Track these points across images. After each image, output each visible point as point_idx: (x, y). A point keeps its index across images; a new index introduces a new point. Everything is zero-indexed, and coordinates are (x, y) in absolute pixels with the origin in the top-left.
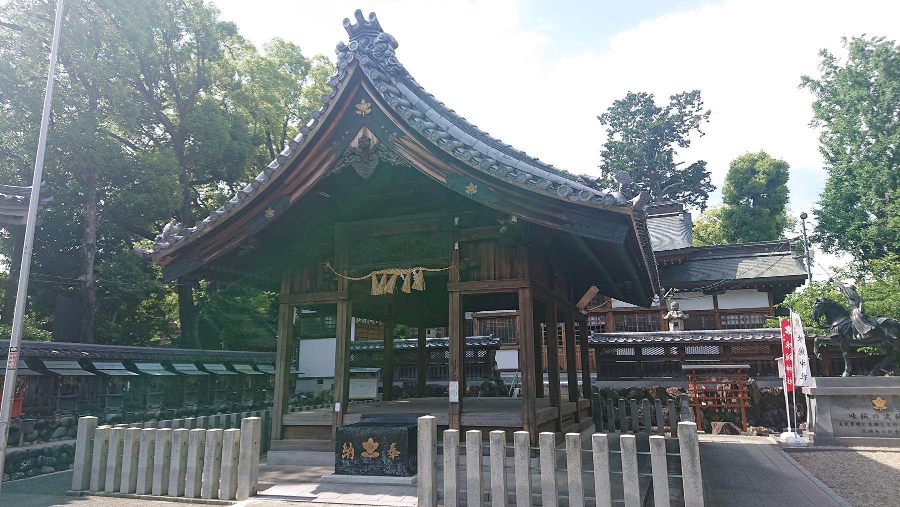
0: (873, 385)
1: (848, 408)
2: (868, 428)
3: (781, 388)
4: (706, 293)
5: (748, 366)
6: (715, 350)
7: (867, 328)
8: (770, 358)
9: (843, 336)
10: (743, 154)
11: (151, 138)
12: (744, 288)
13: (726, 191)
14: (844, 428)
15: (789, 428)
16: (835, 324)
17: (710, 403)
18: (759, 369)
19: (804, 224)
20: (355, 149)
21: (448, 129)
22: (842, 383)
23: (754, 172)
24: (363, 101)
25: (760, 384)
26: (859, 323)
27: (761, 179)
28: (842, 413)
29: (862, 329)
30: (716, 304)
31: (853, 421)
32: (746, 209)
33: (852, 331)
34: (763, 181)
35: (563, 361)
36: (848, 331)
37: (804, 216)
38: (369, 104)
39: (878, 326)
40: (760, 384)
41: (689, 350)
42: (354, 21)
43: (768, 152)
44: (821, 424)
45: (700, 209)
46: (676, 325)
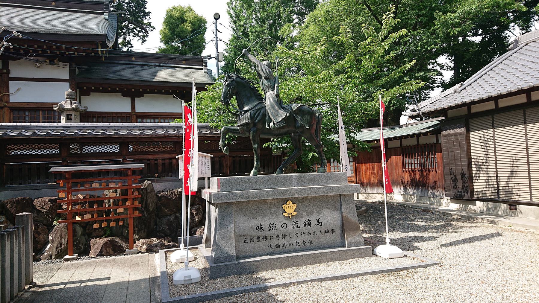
0: (284, 185)
1: (255, 217)
2: (275, 242)
3: (180, 190)
4: (125, 95)
5: (142, 165)
6: (115, 149)
7: (282, 115)
8: (172, 156)
9: (255, 125)
10: (176, 5)
12: (160, 92)
13: (163, 33)
14: (249, 247)
15: (182, 245)
16: (246, 108)
17: (88, 216)
18: (160, 169)
19: (216, 24)
22: (250, 185)
23: (183, 21)
25: (158, 186)
26: (274, 108)
27: (188, 27)
28: (246, 223)
29: (276, 115)
30: (133, 107)
31: (260, 235)
32: (176, 49)
33: (265, 118)
34: (189, 28)
35: (410, 165)
36: (260, 117)
37: (217, 17)
39: (292, 112)
40: (158, 186)
43: (194, 9)
44: (222, 244)
45: (141, 41)
46: (69, 119)
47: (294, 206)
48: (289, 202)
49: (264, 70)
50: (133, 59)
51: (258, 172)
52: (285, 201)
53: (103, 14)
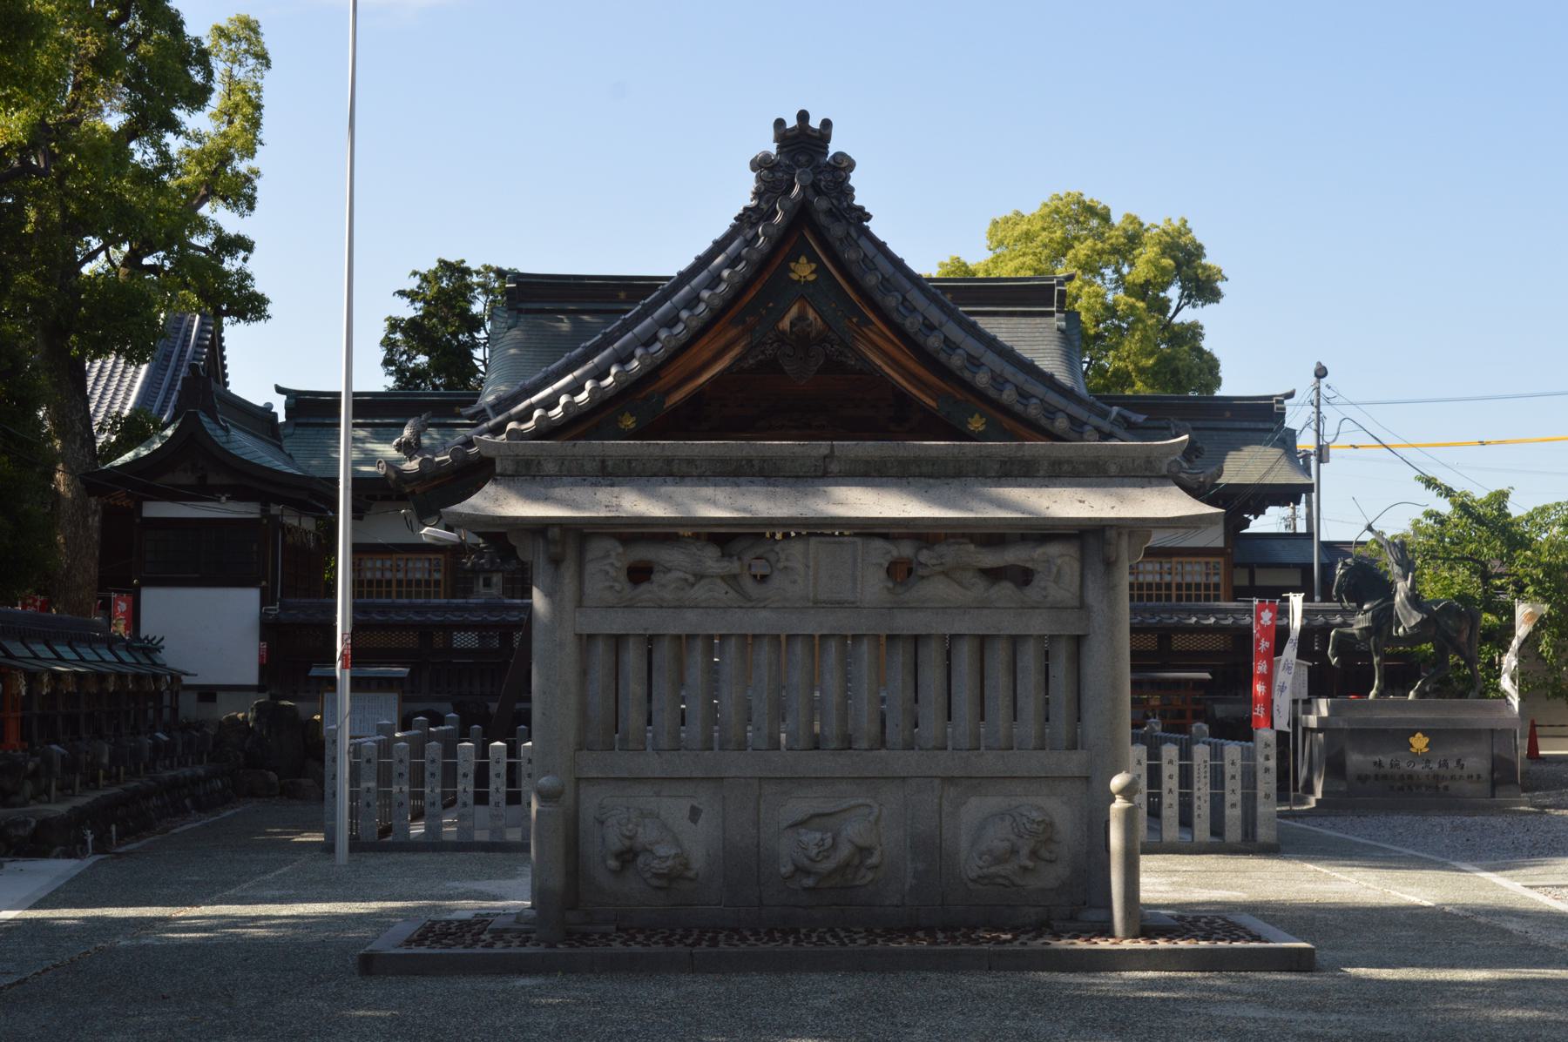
5: (1207, 676)
11: (21, 160)
20: (783, 332)
21: (941, 325)
24: (803, 260)
38: (814, 266)
41: (1179, 642)
42: (791, 122)
47: (1426, 740)
48: (1419, 735)
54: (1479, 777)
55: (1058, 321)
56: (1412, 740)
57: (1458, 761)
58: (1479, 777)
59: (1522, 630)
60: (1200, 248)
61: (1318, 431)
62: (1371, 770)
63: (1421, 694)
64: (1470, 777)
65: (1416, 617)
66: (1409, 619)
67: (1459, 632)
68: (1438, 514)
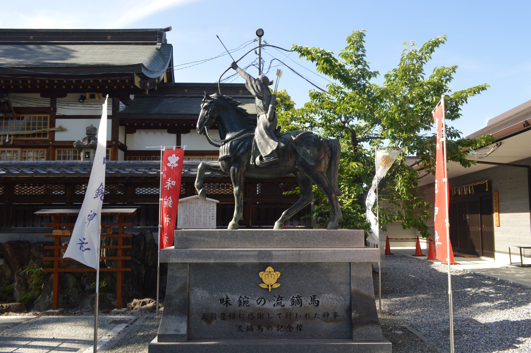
4: (170, 131)
47: (278, 274)
48: (270, 269)
49: (255, 86)
50: (186, 91)
51: (241, 224)
52: (263, 267)
53: (155, 44)
54: (335, 315)
55: (159, 46)
56: (262, 275)
57: (313, 298)
58: (335, 315)
59: (381, 172)
60: (289, 97)
61: (260, 69)
62: (216, 307)
63: (283, 225)
64: (326, 315)
65: (273, 145)
66: (266, 146)
67: (318, 162)
68: (301, 48)
